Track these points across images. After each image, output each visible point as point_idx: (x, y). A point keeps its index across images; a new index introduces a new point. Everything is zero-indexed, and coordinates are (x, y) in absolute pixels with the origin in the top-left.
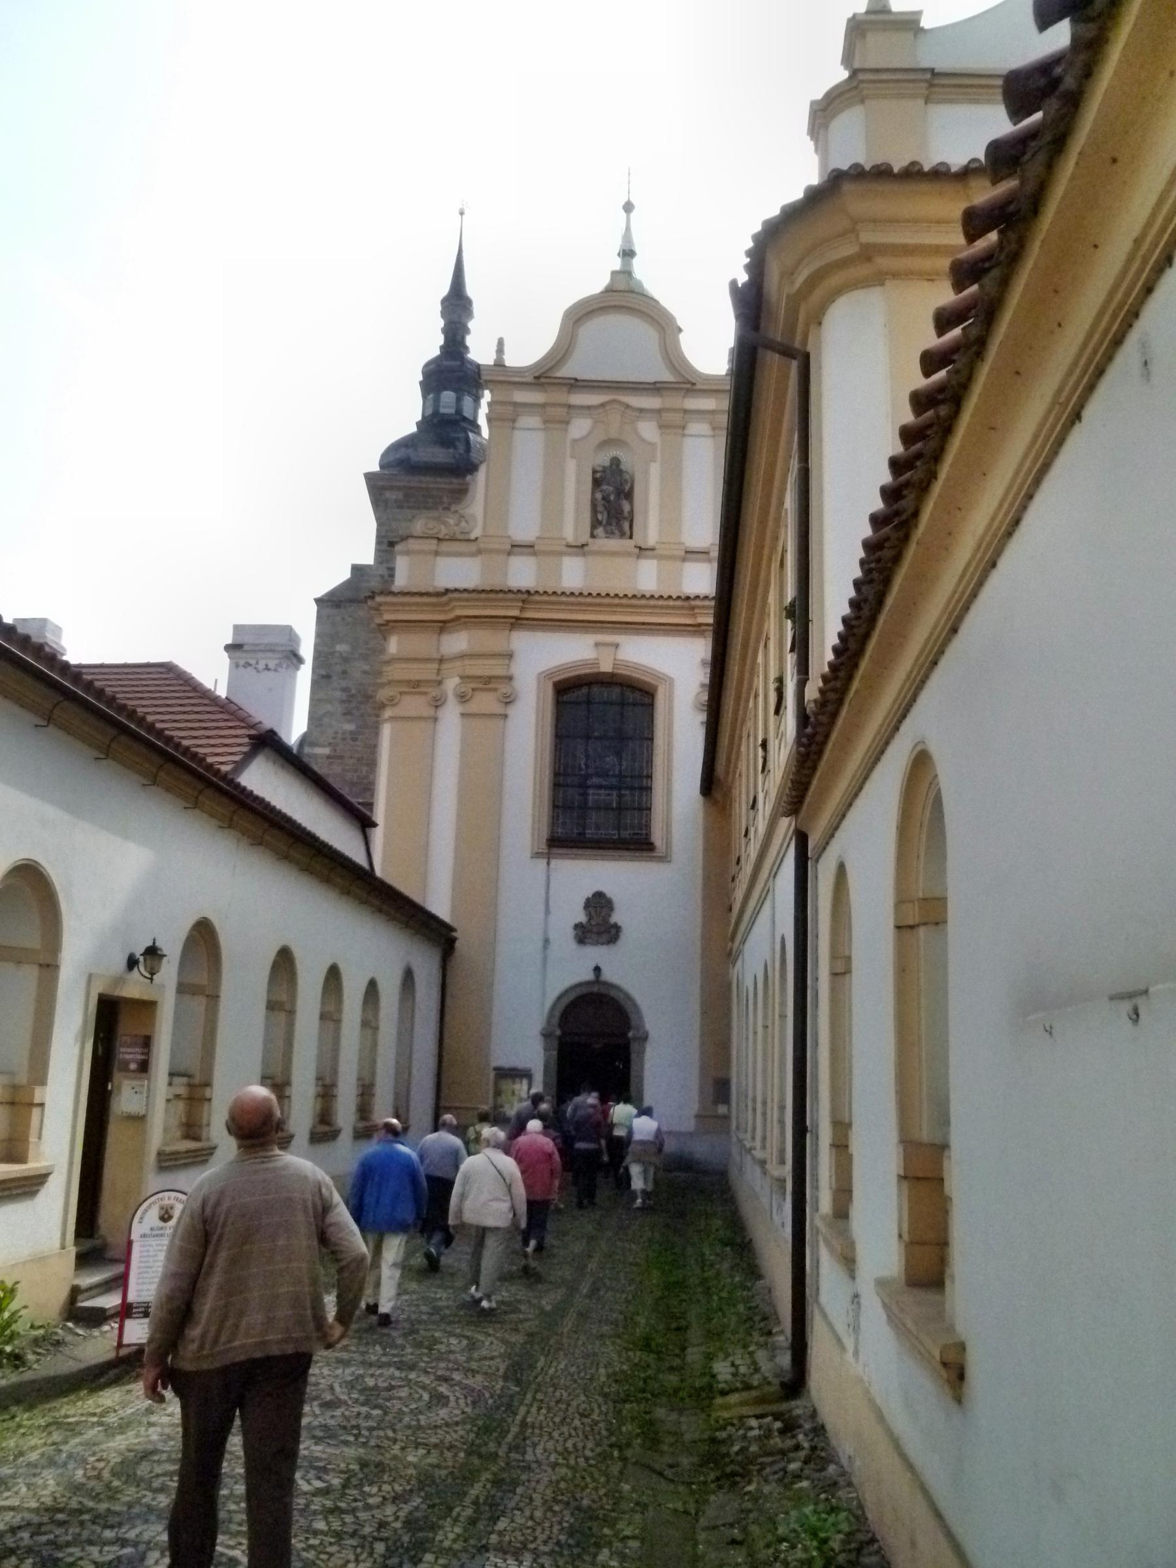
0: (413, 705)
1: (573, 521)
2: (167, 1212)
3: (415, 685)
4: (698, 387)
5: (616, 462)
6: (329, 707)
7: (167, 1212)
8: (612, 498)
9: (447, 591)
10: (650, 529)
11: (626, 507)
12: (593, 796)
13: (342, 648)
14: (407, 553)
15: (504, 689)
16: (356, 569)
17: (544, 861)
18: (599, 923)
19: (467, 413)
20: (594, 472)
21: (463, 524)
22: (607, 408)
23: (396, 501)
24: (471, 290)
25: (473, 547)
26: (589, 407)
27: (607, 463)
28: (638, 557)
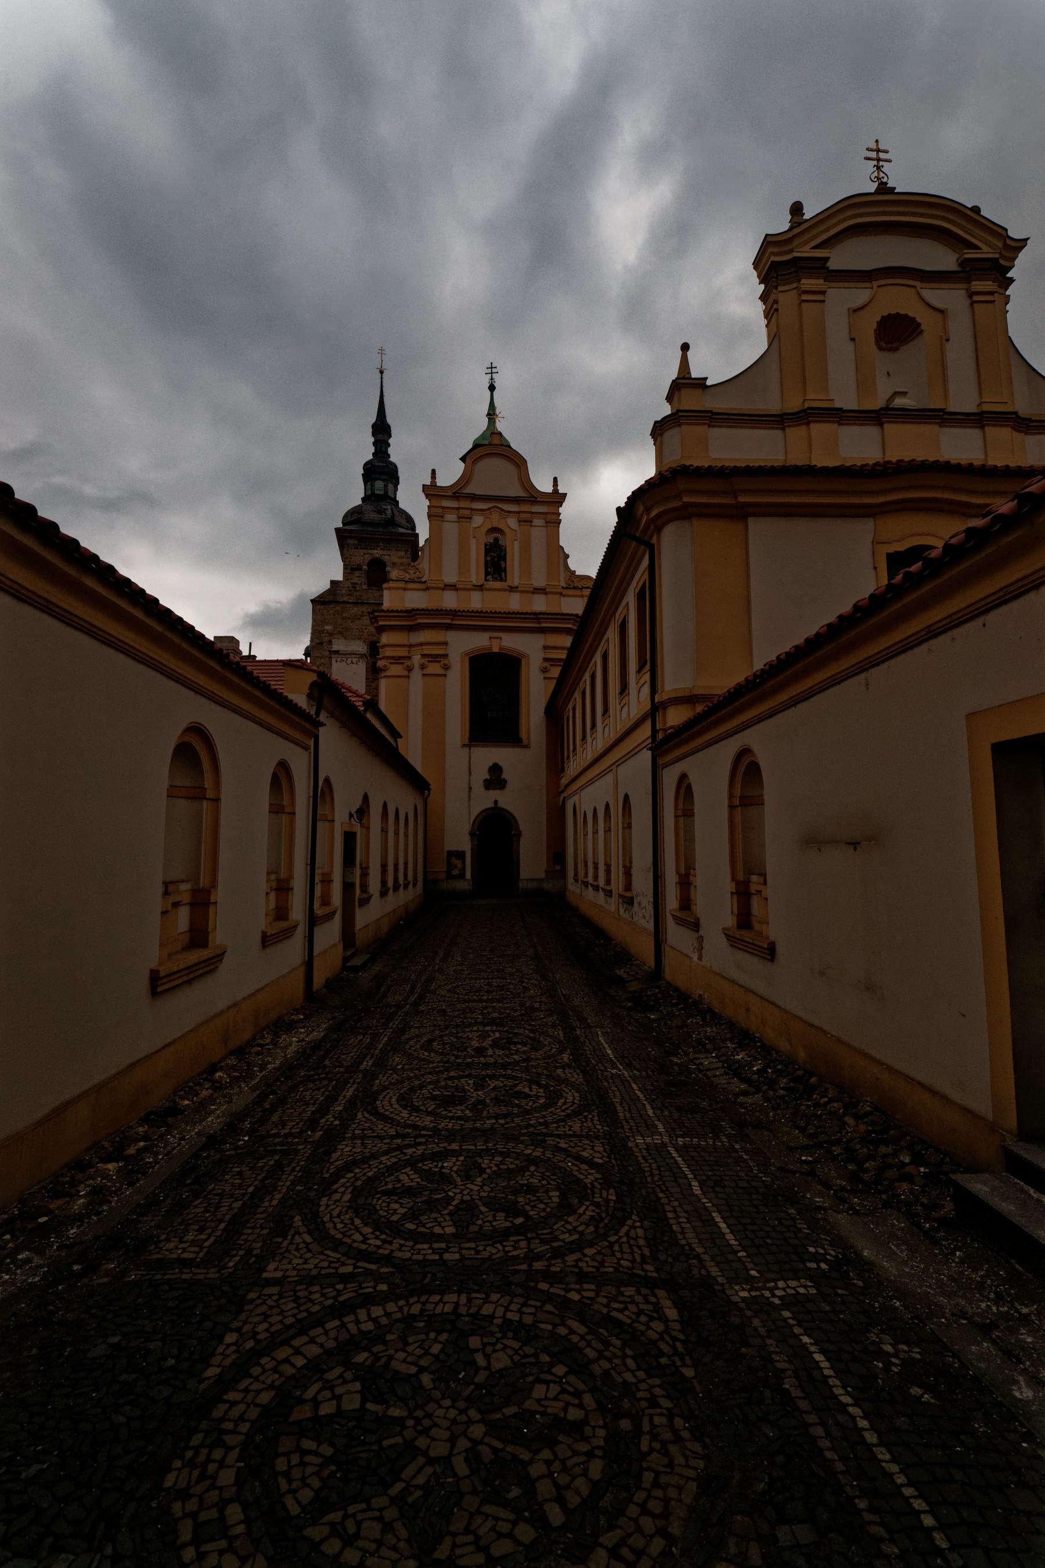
0: (396, 670)
1: (476, 574)
3: (397, 660)
6: (323, 660)
9: (413, 610)
10: (515, 576)
11: (503, 565)
13: (328, 627)
16: (333, 582)
18: (496, 779)
19: (391, 494)
26: (482, 510)
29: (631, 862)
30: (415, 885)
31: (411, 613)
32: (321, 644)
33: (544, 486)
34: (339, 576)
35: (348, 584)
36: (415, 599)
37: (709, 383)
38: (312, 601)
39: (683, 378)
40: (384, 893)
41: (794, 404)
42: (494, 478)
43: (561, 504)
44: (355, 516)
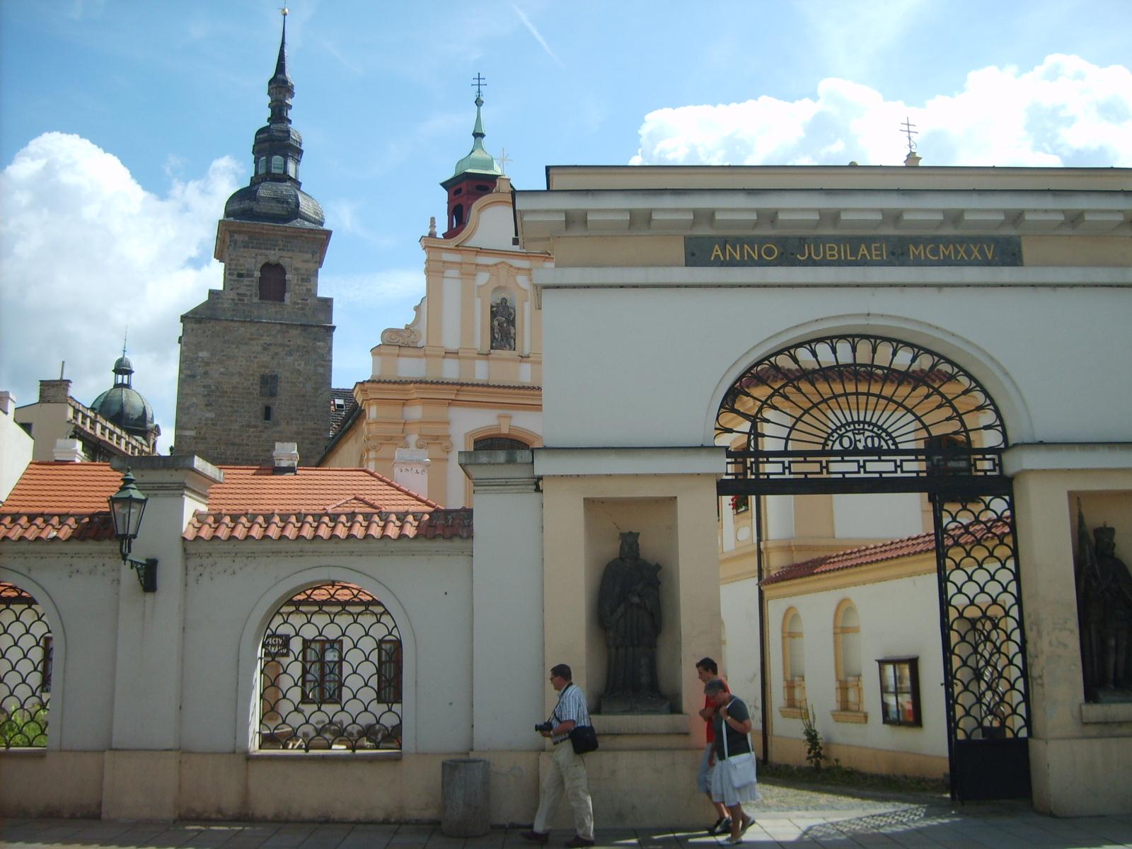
1: (480, 338)
5: (504, 300)
6: (194, 400)
8: (505, 325)
11: (512, 331)
13: (204, 354)
15: (445, 444)
16: (212, 293)
19: (292, 173)
20: (492, 307)
21: (413, 336)
23: (243, 242)
24: (290, 74)
25: (422, 352)
26: (487, 266)
27: (499, 301)
28: (521, 362)
32: (193, 376)
34: (219, 286)
35: (233, 295)
44: (246, 204)
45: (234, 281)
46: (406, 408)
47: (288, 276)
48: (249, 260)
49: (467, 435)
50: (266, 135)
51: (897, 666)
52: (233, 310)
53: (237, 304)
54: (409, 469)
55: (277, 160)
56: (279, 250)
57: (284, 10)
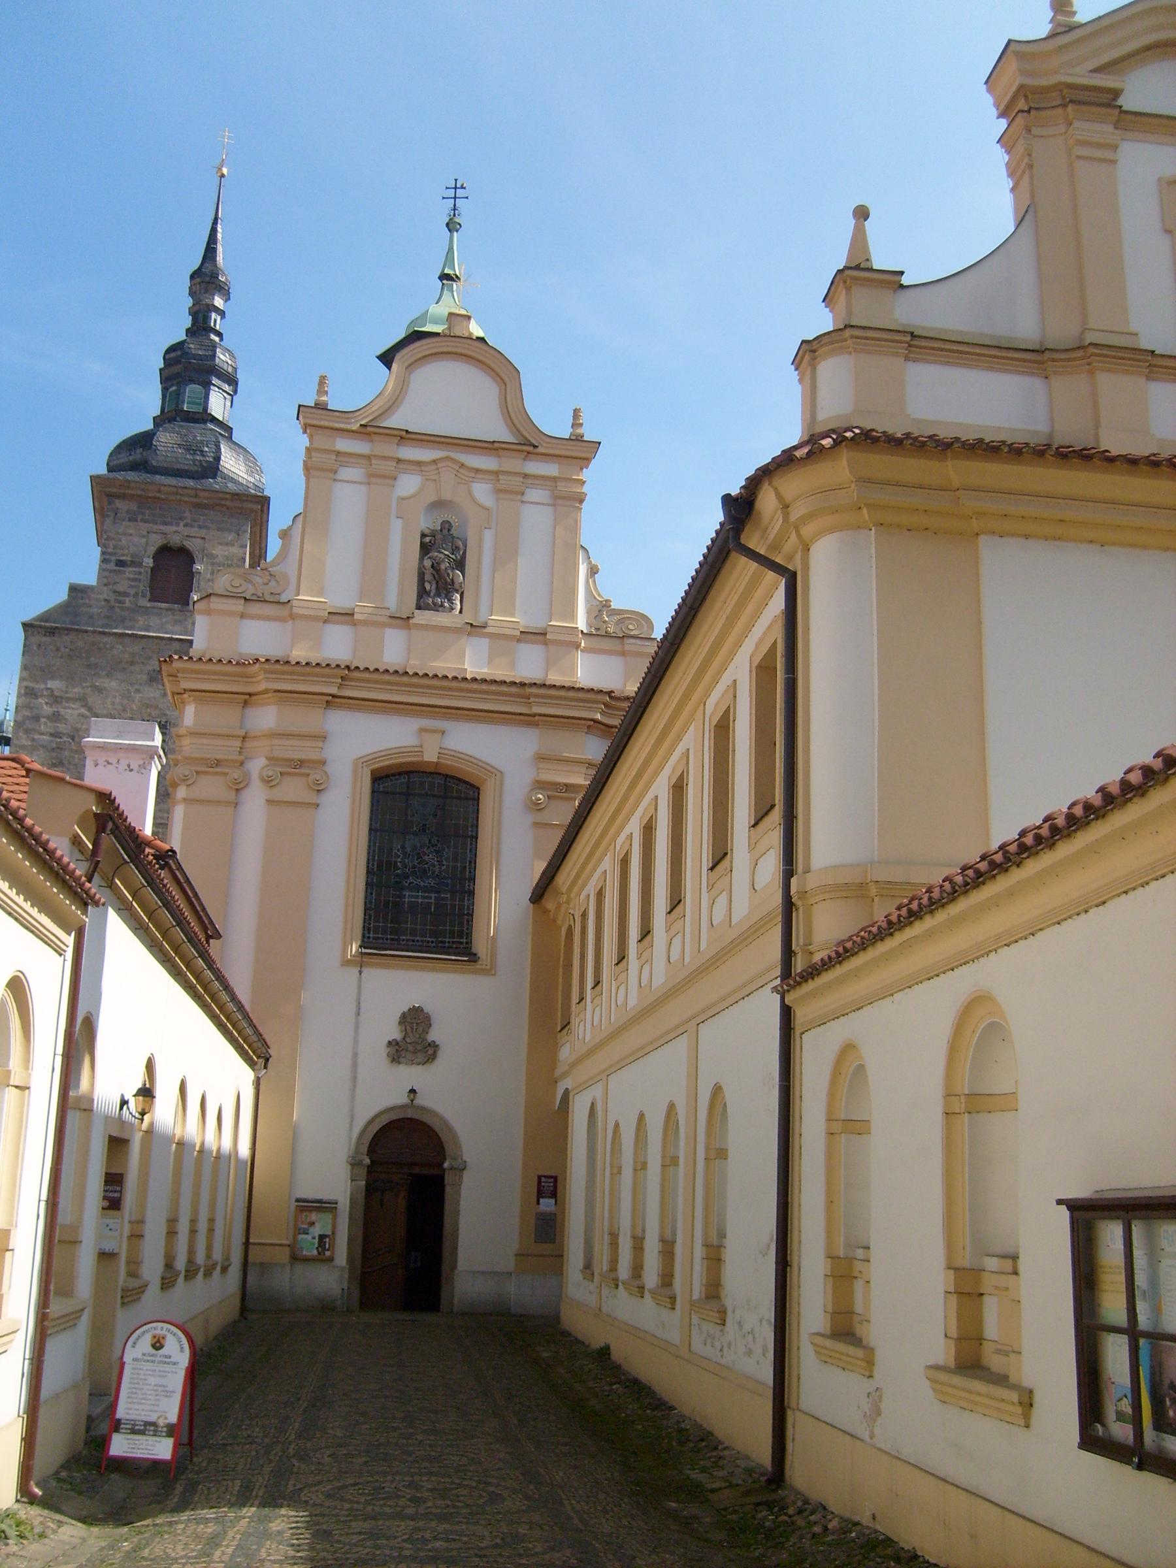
1: (397, 588)
2: (158, 1341)
4: (540, 450)
5: (447, 526)
7: (158, 1341)
12: (408, 897)
14: (208, 613)
15: (315, 775)
16: (74, 589)
17: (356, 970)
18: (414, 1040)
20: (423, 535)
21: (273, 583)
22: (440, 465)
23: (128, 512)
26: (419, 463)
29: (722, 1235)
30: (224, 1269)
31: (245, 665)
33: (553, 423)
34: (88, 572)
36: (258, 637)
37: (905, 281)
38: (26, 625)
39: (857, 268)
40: (167, 1284)
41: (1063, 331)
42: (446, 400)
43: (585, 461)
44: (138, 455)
45: (111, 571)
46: (249, 710)
47: (198, 567)
48: (136, 539)
49: (359, 763)
50: (179, 353)
51: (1137, 1229)
52: (107, 617)
53: (112, 608)
54: (113, 760)
55: (192, 390)
56: (185, 525)
57: (220, 169)
